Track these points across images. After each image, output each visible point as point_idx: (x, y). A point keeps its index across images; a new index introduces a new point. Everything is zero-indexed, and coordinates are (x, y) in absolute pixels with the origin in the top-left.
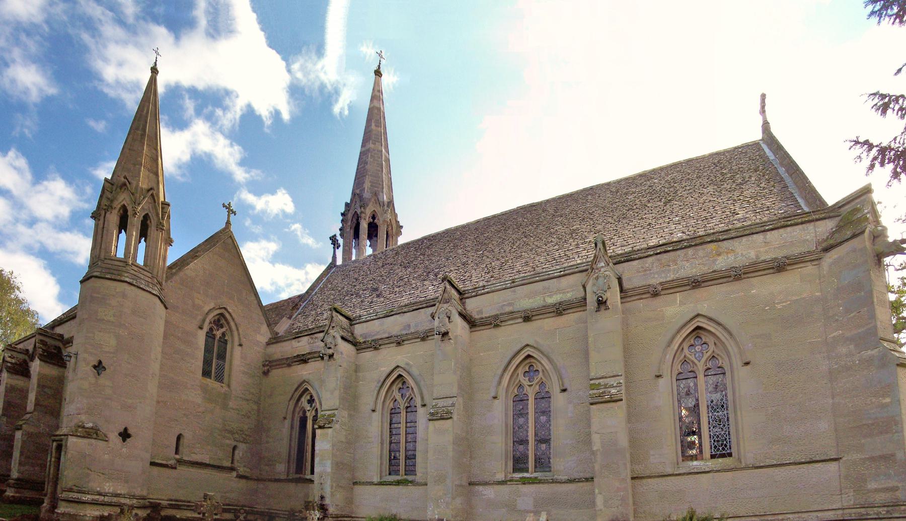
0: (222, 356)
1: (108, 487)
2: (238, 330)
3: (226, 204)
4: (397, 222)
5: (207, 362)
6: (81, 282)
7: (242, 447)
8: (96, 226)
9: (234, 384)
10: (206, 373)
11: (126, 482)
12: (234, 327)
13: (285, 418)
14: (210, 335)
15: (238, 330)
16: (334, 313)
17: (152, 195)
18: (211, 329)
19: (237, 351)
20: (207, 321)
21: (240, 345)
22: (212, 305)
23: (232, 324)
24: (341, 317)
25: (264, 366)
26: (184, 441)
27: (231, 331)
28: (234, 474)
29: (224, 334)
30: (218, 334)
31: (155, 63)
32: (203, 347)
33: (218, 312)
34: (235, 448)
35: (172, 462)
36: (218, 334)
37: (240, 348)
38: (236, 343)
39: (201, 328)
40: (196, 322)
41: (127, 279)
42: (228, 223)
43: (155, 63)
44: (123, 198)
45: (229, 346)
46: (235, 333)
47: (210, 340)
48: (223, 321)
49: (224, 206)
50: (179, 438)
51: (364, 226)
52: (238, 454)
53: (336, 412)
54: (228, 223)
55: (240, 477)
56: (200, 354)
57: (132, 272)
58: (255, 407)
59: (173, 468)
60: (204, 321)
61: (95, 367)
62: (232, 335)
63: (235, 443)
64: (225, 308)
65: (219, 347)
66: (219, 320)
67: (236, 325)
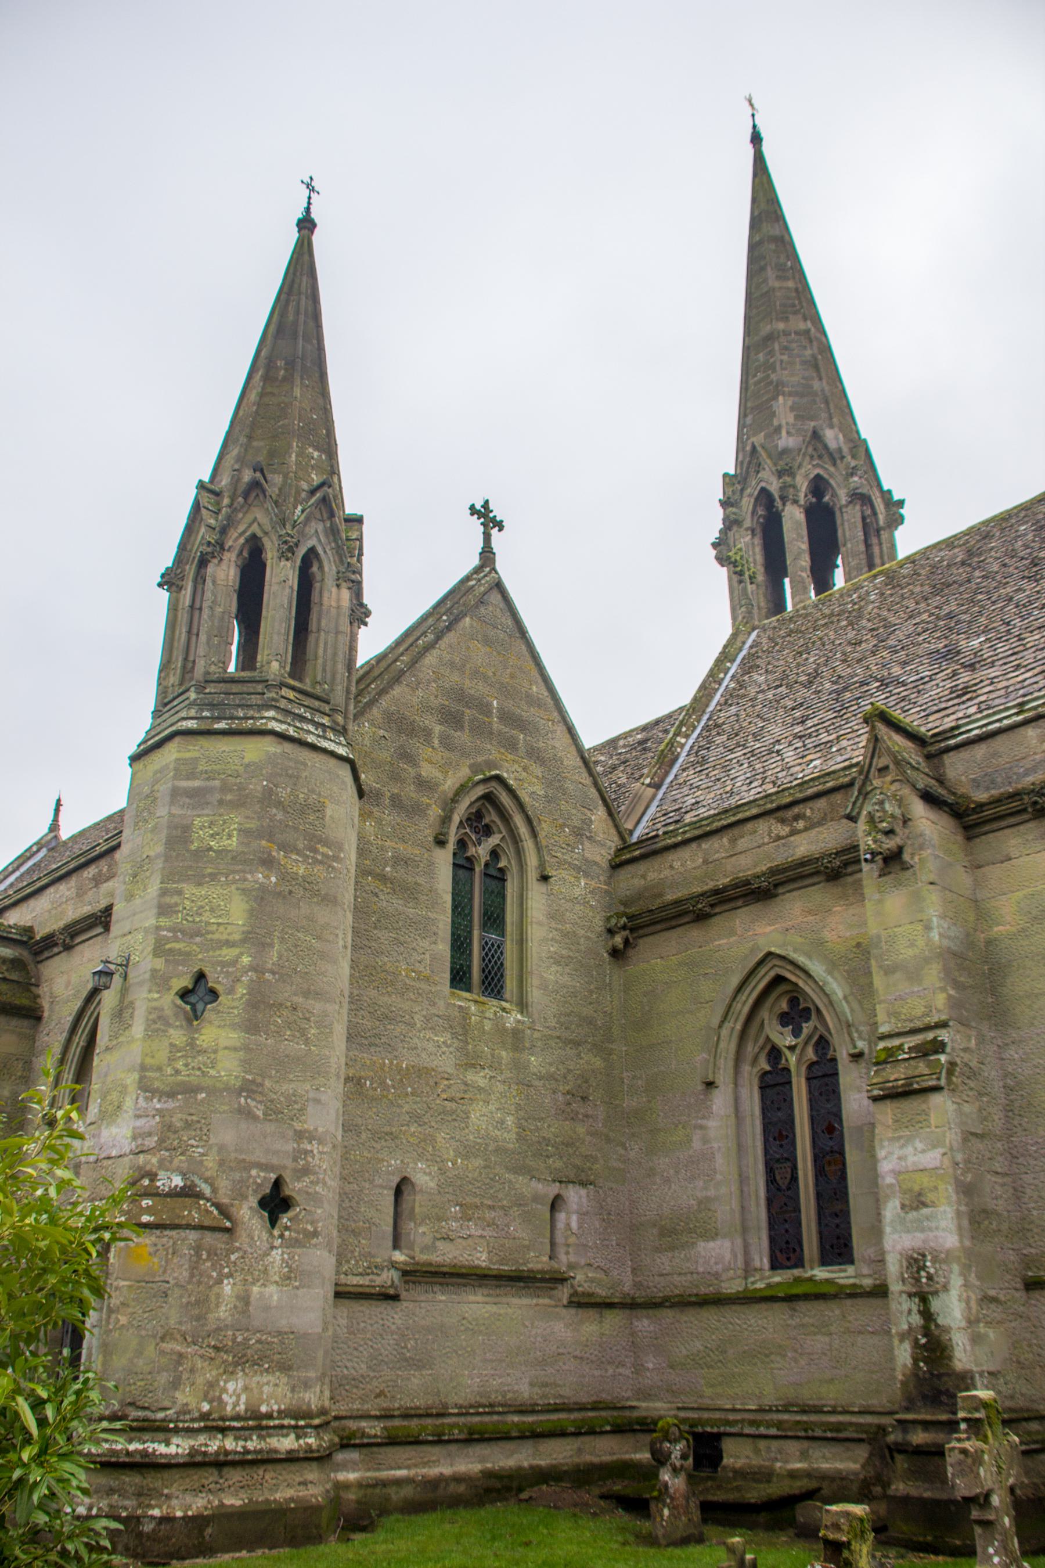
0: (494, 919)
1: (234, 1394)
2: (534, 834)
3: (478, 507)
4: (887, 495)
5: (460, 944)
6: (135, 759)
7: (575, 1196)
8: (173, 608)
9: (535, 995)
10: (459, 978)
11: (285, 1368)
12: (523, 830)
13: (710, 1085)
14: (463, 865)
15: (534, 834)
16: (882, 729)
17: (324, 500)
18: (462, 844)
19: (537, 901)
20: (456, 819)
21: (545, 878)
22: (464, 772)
23: (518, 820)
24: (898, 738)
25: (611, 932)
26: (417, 1203)
27: (516, 839)
28: (564, 1293)
29: (495, 854)
30: (481, 852)
31: (308, 210)
32: (448, 898)
33: (480, 791)
34: (556, 1204)
35: (388, 1278)
36: (481, 852)
37: (542, 888)
38: (532, 874)
39: (441, 843)
40: (428, 834)
41: (274, 725)
42: (487, 555)
43: (308, 210)
44: (258, 519)
45: (511, 888)
46: (528, 845)
47: (461, 873)
48: (491, 816)
49: (473, 510)
50: (400, 1189)
51: (794, 519)
52: (569, 1220)
53: (944, 1035)
54: (487, 555)
55: (582, 1303)
56: (444, 921)
57: (283, 703)
58: (598, 1063)
59: (390, 1297)
60: (446, 820)
61: (184, 994)
62: (519, 853)
63: (554, 1189)
64: (498, 778)
65: (486, 891)
66: (479, 815)
67: (529, 821)
